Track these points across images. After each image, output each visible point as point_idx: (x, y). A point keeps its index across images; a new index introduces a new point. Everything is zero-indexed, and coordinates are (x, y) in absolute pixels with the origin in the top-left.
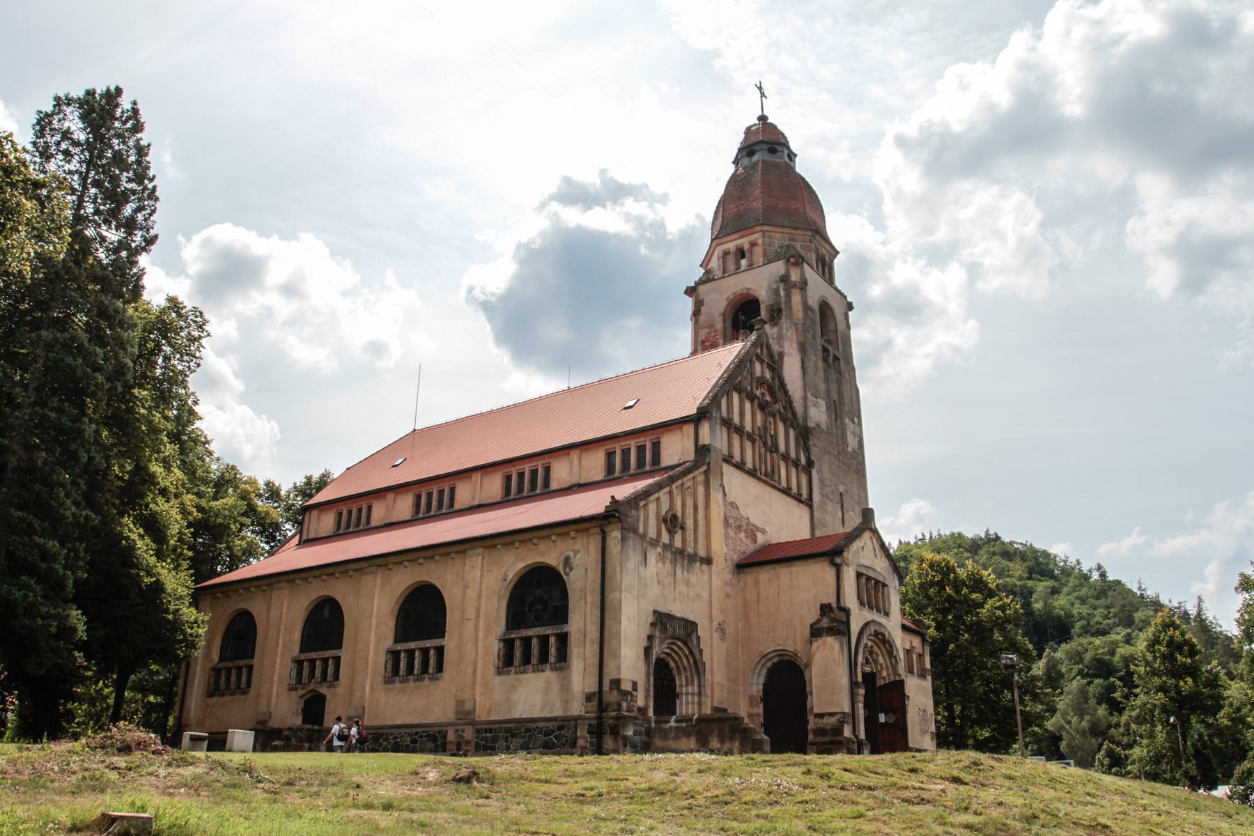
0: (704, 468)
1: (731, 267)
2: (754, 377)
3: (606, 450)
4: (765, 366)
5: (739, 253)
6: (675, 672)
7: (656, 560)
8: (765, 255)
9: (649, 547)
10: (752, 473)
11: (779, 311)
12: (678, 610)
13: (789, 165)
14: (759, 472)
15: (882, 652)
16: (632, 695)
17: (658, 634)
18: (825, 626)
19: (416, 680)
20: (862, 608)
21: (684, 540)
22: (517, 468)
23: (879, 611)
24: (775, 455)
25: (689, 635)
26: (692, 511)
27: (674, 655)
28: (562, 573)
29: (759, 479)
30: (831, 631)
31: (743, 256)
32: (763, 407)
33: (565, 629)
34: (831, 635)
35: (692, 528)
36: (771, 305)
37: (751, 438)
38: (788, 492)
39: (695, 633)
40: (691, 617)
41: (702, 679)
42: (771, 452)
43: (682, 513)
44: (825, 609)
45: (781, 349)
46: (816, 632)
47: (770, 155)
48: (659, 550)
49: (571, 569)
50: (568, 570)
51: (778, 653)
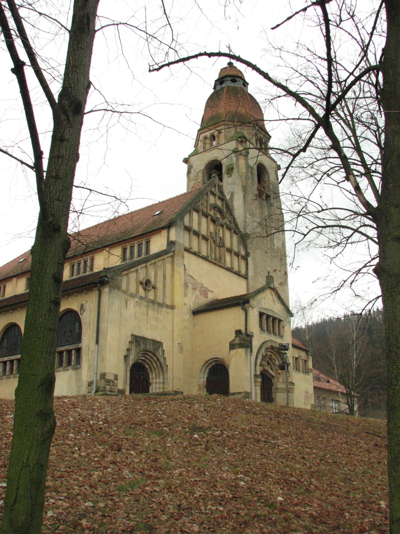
0: (171, 254)
1: (208, 146)
2: (208, 203)
3: (122, 247)
4: (217, 197)
5: (212, 138)
6: (149, 370)
7: (135, 306)
8: (225, 138)
9: (129, 298)
10: (205, 258)
11: (232, 168)
12: (149, 334)
13: (243, 90)
14: (210, 258)
15: (277, 358)
16: (113, 382)
17: (133, 348)
18: (237, 342)
19: (7, 378)
20: (263, 332)
21: (155, 295)
22: (78, 260)
23: (274, 333)
24: (222, 248)
25: (157, 349)
26: (162, 278)
27: (147, 361)
28: (79, 314)
29: (211, 262)
30: (241, 346)
31: (214, 139)
32: (214, 221)
33: (80, 345)
34: (241, 348)
35: (162, 288)
36: (228, 166)
37: (205, 238)
38: (239, 273)
39: (161, 348)
40: (158, 339)
41: (165, 375)
42: (219, 247)
43: (155, 281)
44: (238, 332)
45: (233, 190)
46: (232, 346)
47: (233, 83)
48: (137, 299)
49: (84, 311)
50: (82, 312)
51: (214, 360)
